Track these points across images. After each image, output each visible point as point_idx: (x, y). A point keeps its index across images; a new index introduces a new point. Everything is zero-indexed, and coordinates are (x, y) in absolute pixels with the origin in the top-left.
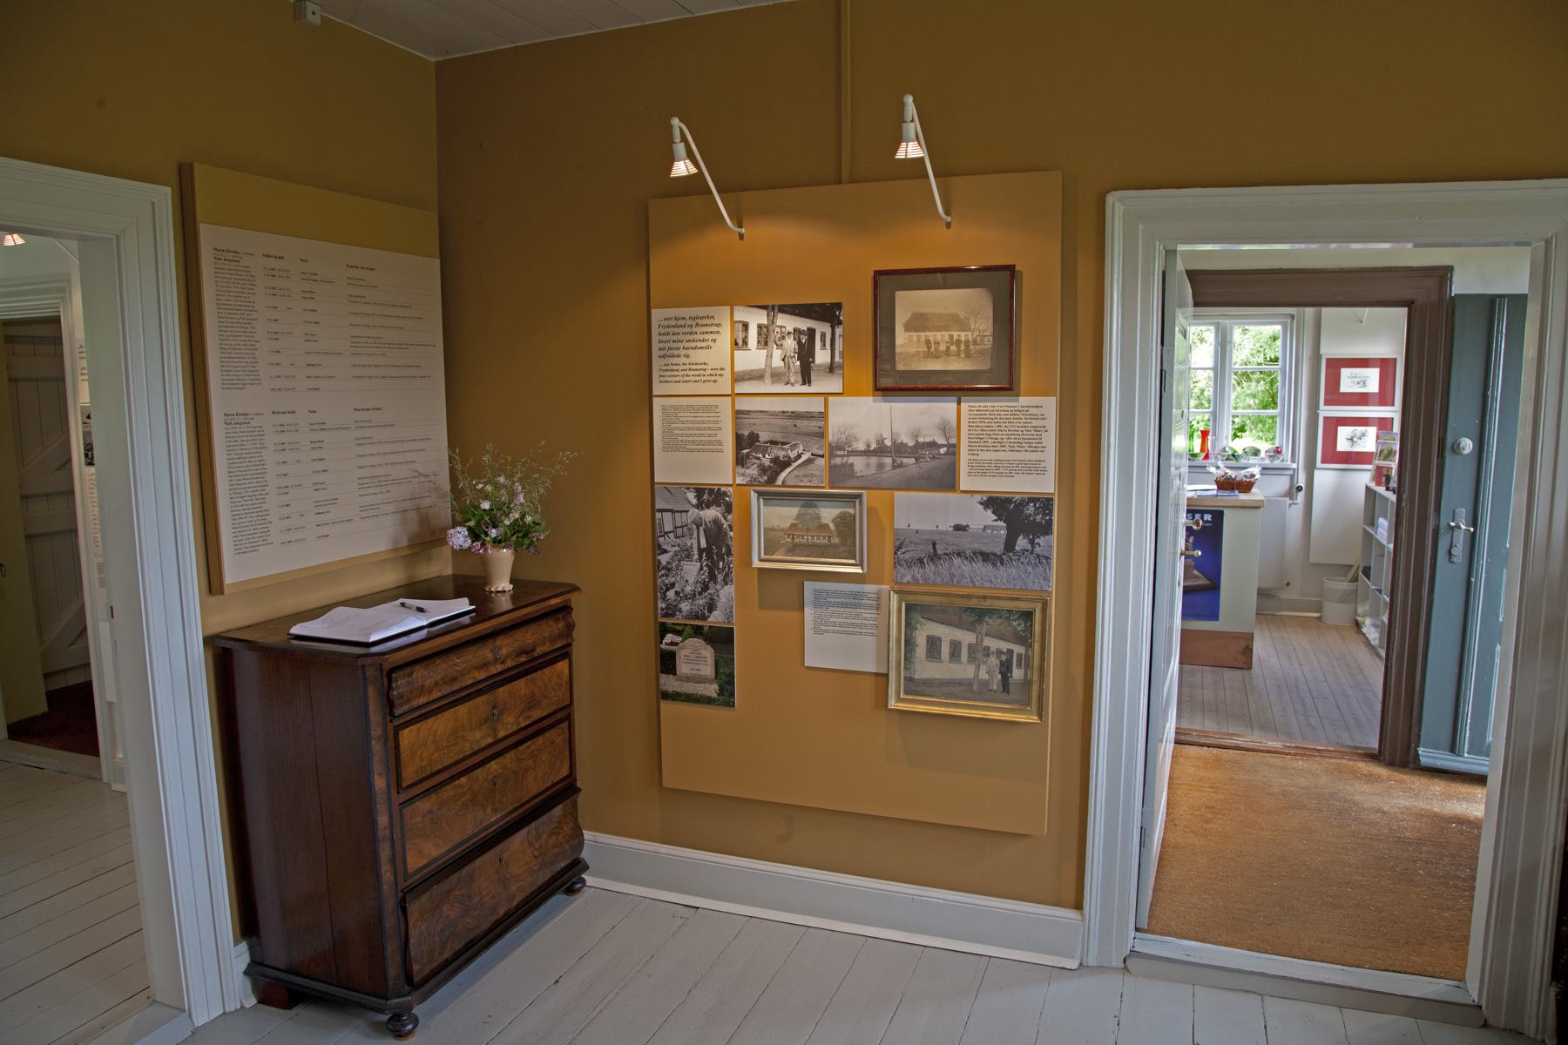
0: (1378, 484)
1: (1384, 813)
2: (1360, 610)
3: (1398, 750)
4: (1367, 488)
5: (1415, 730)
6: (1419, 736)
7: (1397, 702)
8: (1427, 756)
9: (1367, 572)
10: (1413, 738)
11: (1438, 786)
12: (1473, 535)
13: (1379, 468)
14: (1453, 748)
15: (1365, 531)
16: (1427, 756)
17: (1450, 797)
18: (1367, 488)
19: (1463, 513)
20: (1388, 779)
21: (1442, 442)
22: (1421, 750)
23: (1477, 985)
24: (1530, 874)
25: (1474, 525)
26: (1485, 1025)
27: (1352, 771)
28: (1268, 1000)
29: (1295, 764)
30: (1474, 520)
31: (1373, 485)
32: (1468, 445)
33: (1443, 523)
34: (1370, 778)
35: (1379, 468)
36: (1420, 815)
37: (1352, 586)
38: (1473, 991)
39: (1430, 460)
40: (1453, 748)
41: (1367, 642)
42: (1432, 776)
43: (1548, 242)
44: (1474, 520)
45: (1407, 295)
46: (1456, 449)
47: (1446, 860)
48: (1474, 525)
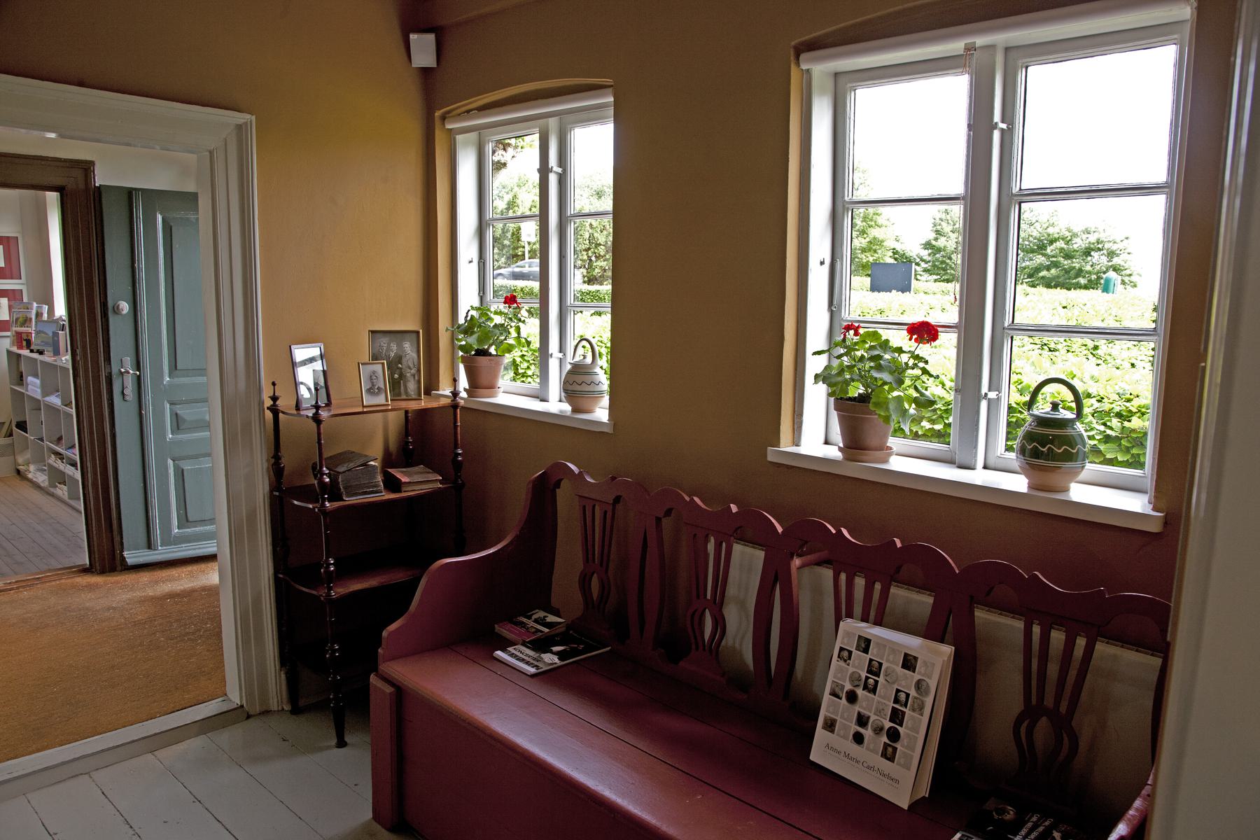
0: (20, 347)
1: (114, 609)
2: (20, 460)
3: (107, 558)
4: (8, 351)
5: (117, 539)
6: (122, 544)
7: (98, 520)
8: (131, 557)
9: (22, 426)
10: (117, 546)
11: (145, 577)
12: (139, 377)
13: (19, 334)
14: (149, 546)
15: (13, 391)
16: (131, 557)
17: (157, 582)
18: (8, 351)
19: (128, 362)
20: (106, 584)
21: (104, 305)
22: (125, 554)
23: (238, 693)
24: (257, 601)
25: (138, 369)
26: (249, 717)
27: (73, 586)
28: (95, 775)
29: (21, 596)
30: (138, 366)
31: (15, 349)
32: (125, 307)
33: (115, 370)
34: (91, 588)
35: (19, 335)
36: (143, 601)
37: (8, 440)
38: (235, 697)
39: (95, 320)
40: (149, 546)
41: (37, 486)
42: (154, 570)
43: (211, 153)
44: (138, 366)
45: (59, 181)
46: (117, 310)
47: (175, 625)
48: (138, 369)
